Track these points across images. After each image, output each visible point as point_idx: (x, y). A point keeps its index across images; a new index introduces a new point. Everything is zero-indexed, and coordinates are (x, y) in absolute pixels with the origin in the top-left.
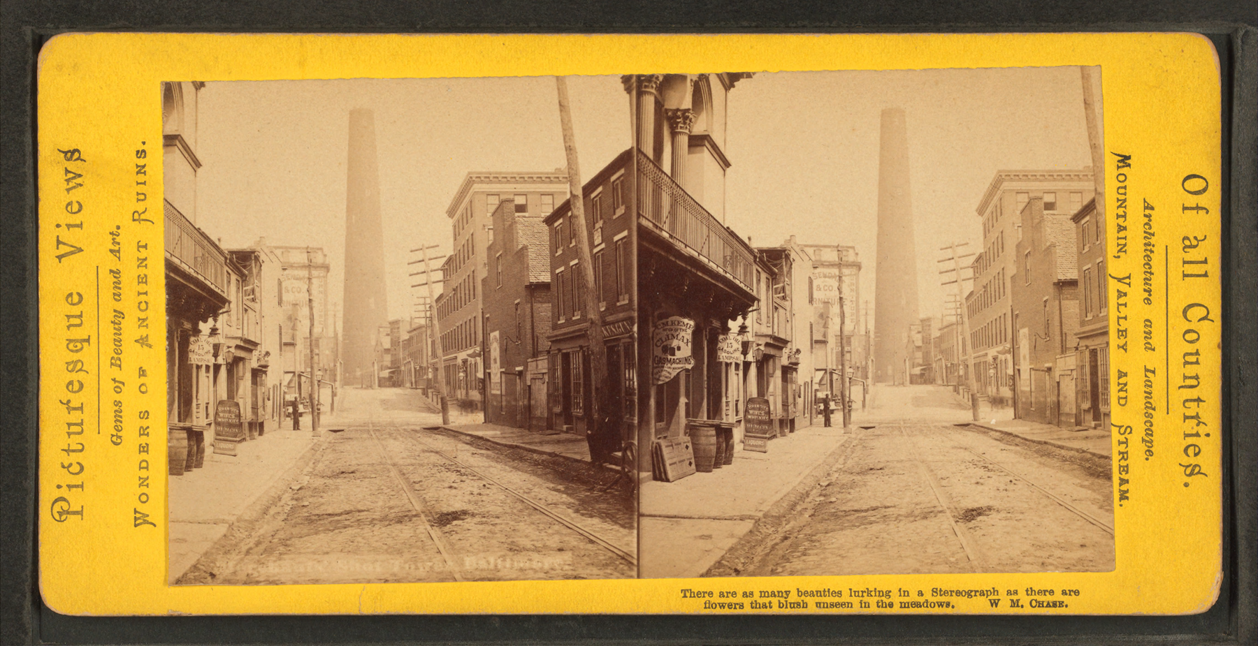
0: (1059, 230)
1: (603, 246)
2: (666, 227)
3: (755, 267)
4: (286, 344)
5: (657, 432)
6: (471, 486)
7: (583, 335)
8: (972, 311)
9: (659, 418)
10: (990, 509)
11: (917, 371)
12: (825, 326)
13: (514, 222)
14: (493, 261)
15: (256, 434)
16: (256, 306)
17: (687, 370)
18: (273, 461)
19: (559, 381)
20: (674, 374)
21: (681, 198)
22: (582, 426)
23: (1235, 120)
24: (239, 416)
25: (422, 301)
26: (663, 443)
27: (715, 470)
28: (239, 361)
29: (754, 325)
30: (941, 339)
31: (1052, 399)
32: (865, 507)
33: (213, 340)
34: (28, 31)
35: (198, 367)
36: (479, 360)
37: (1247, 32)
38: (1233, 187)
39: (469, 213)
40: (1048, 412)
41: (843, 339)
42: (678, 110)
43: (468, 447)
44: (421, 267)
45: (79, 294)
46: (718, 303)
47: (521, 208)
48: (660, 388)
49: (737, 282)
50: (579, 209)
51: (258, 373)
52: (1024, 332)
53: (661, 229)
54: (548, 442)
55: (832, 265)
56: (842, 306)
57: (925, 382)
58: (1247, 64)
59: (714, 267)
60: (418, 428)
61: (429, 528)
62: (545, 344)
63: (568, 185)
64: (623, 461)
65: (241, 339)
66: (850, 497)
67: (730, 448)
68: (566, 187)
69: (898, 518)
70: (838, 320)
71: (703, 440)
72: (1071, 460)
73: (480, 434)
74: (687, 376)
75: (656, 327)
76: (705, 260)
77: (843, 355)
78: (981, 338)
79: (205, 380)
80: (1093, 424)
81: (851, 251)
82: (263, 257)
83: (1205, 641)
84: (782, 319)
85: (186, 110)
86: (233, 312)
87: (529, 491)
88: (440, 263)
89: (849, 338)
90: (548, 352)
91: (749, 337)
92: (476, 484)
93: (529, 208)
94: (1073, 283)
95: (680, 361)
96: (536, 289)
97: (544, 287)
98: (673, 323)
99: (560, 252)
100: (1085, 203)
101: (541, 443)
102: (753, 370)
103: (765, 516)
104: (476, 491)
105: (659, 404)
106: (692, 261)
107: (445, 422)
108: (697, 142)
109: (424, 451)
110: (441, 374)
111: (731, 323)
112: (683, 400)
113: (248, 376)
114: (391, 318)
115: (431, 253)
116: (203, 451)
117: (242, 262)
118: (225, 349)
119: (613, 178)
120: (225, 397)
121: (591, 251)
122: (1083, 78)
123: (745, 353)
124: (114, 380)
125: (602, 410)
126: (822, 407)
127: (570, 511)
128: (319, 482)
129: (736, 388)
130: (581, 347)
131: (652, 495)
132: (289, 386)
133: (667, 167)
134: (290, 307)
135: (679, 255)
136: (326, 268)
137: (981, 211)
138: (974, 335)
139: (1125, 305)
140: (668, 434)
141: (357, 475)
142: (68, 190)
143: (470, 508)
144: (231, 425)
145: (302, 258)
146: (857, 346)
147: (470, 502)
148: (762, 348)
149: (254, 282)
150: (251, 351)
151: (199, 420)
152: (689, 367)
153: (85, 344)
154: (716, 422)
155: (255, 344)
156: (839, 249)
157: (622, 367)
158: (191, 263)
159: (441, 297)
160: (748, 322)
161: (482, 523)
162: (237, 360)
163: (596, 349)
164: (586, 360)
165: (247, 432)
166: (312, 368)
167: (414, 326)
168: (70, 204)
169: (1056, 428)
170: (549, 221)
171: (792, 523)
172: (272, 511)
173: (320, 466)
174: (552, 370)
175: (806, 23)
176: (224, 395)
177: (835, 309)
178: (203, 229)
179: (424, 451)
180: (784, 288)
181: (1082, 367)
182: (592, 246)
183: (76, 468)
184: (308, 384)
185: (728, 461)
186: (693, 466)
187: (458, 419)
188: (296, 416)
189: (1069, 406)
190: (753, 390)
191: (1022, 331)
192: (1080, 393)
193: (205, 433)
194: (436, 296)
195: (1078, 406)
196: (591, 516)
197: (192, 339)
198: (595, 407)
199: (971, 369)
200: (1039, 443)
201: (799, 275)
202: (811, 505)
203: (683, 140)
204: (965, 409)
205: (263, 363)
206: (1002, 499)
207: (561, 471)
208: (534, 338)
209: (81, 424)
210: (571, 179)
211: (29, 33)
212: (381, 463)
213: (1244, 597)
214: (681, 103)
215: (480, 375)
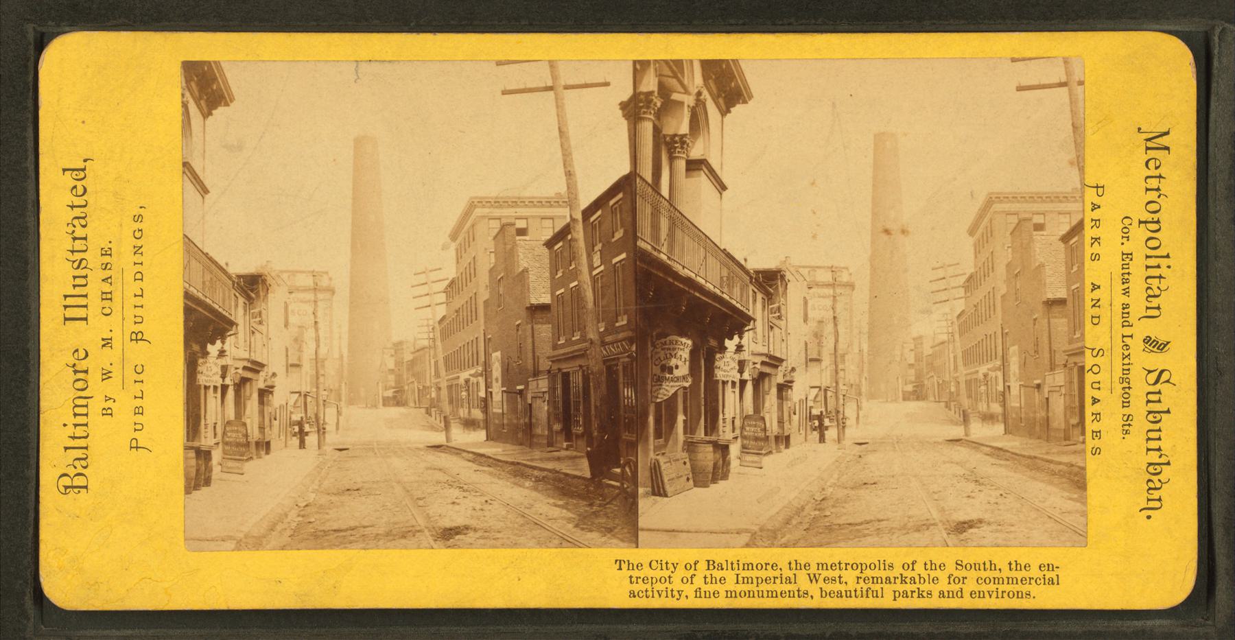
0: (1047, 249)
1: (602, 268)
2: (664, 249)
3: (751, 287)
4: (292, 365)
5: (656, 448)
6: (474, 501)
7: (583, 355)
8: (964, 329)
9: (658, 435)
10: (980, 521)
11: (910, 388)
12: (300, 350)
13: (515, 244)
15: (782, 447)
16: (263, 328)
17: (685, 388)
18: (284, 475)
19: (560, 400)
20: (673, 391)
21: (679, 222)
22: (582, 443)
23: (1213, 116)
24: (247, 436)
25: (425, 323)
26: (662, 460)
27: (713, 486)
28: (247, 381)
29: (753, 343)
30: (413, 363)
31: (1041, 414)
32: (859, 521)
33: (223, 362)
34: (30, 30)
35: (206, 388)
36: (481, 380)
37: (1224, 29)
38: (1211, 181)
39: (471, 238)
40: (1037, 428)
41: (318, 361)
42: (676, 135)
43: (470, 464)
44: (424, 290)
46: (715, 322)
47: (522, 232)
48: (658, 405)
49: (734, 302)
50: (579, 233)
51: (264, 394)
52: (1014, 349)
53: (660, 252)
54: (549, 459)
55: (306, 290)
56: (836, 325)
57: (918, 399)
58: (1225, 60)
59: (711, 287)
60: (421, 446)
61: (945, 535)
62: (1060, 359)
63: (568, 209)
64: (622, 478)
65: (248, 360)
66: (327, 517)
67: (726, 463)
68: (566, 212)
69: (891, 531)
70: (312, 346)
71: (700, 456)
72: (1061, 474)
73: (999, 445)
74: (685, 395)
75: (654, 345)
76: (702, 281)
77: (837, 372)
78: (970, 356)
79: (212, 404)
80: (565, 444)
81: (325, 277)
82: (788, 276)
84: (778, 340)
85: (195, 139)
86: (241, 335)
87: (530, 507)
88: (962, 279)
89: (323, 361)
90: (1065, 366)
91: (745, 355)
92: (478, 499)
93: (530, 231)
94: (1061, 302)
95: (678, 379)
96: (537, 310)
97: (544, 308)
98: (671, 342)
99: (560, 274)
100: (557, 229)
101: (1059, 453)
102: (749, 388)
103: (246, 537)
104: (478, 507)
105: (658, 421)
106: (689, 282)
107: (448, 439)
108: (695, 166)
109: (427, 469)
110: (444, 392)
111: (727, 343)
112: (681, 418)
113: (255, 396)
114: (395, 339)
115: (434, 276)
116: (729, 464)
117: (252, 286)
118: (751, 366)
119: (612, 202)
120: (751, 412)
121: (590, 273)
122: (557, 107)
123: (741, 371)
125: (602, 429)
126: (817, 423)
127: (570, 526)
128: (324, 500)
129: (732, 405)
130: (581, 367)
131: (650, 510)
132: (295, 406)
133: (665, 191)
134: (296, 330)
135: (676, 275)
136: (332, 291)
137: (972, 232)
138: (446, 359)
140: (667, 451)
141: (362, 492)
143: (473, 523)
144: (238, 445)
145: (309, 282)
146: (330, 369)
147: (986, 511)
148: (758, 366)
149: (260, 306)
150: (777, 367)
151: (207, 440)
152: (687, 385)
154: (713, 438)
155: (262, 365)
156: (832, 269)
157: (621, 386)
158: (200, 287)
159: (444, 318)
160: (744, 342)
161: (997, 531)
162: (244, 381)
163: (595, 369)
164: (586, 379)
165: (773, 445)
166: (837, 383)
167: (417, 347)
169: (528, 450)
170: (549, 244)
171: (788, 536)
172: (279, 528)
173: (326, 483)
174: (552, 389)
175: (792, 20)
176: (749, 410)
177: (829, 328)
178: (211, 254)
179: (427, 469)
180: (779, 308)
181: (1071, 382)
182: (591, 268)
184: (314, 403)
185: (725, 476)
186: (691, 482)
187: (979, 430)
188: (302, 434)
189: (1058, 421)
190: (231, 413)
191: (494, 355)
192: (1068, 409)
193: (213, 453)
194: (439, 318)
195: (1067, 422)
196: (591, 531)
197: (201, 361)
198: (595, 424)
199: (963, 386)
200: (1030, 457)
201: (794, 295)
202: (807, 520)
203: (681, 165)
204: (437, 430)
205: (788, 378)
206: (993, 512)
207: (562, 487)
208: (1051, 352)
210: (571, 202)
211: (31, 30)
212: (902, 474)
213: (1222, 584)
214: (678, 128)
215: (482, 394)
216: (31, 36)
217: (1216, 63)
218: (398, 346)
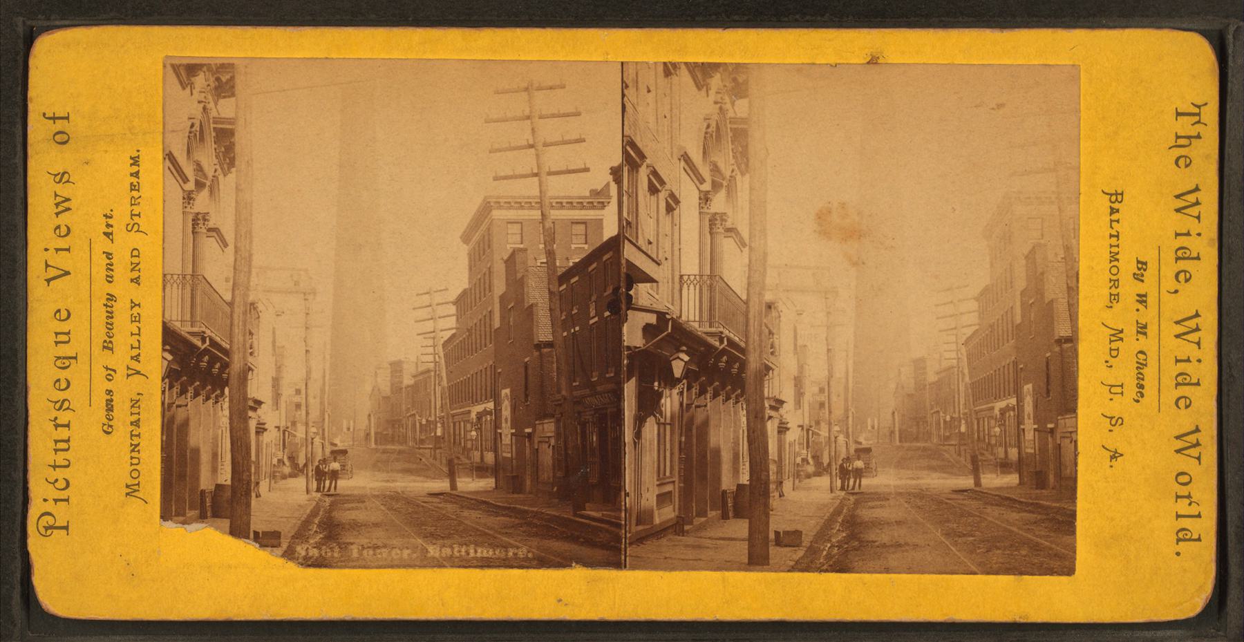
30: (415, 388)
34: (20, 24)
52: (1028, 388)
83: (1194, 637)
115: (438, 298)
124: (107, 369)
139: (1118, 221)
142: (57, 214)
153: (73, 361)
168: (58, 227)
183: (61, 484)
209: (68, 441)
211: (20, 24)
213: (1234, 592)
216: (20, 29)
217: (1230, 63)
218: (396, 367)
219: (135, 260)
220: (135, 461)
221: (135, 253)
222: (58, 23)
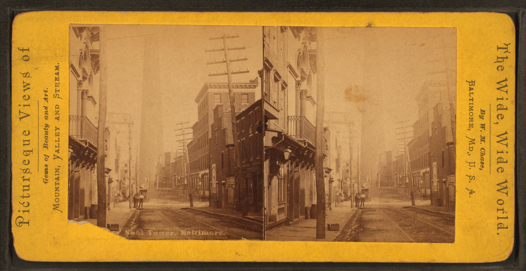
14: (213, 132)
30: (175, 164)
45: (29, 97)
52: (435, 164)
83: (505, 269)
124: (45, 156)
142: (24, 90)
153: (31, 152)
168: (25, 96)
175: (337, 7)
183: (26, 204)
213: (522, 250)
216: (9, 12)
217: (520, 27)
218: (168, 155)
219: (57, 110)
220: (57, 195)
221: (57, 107)
222: (24, 10)
